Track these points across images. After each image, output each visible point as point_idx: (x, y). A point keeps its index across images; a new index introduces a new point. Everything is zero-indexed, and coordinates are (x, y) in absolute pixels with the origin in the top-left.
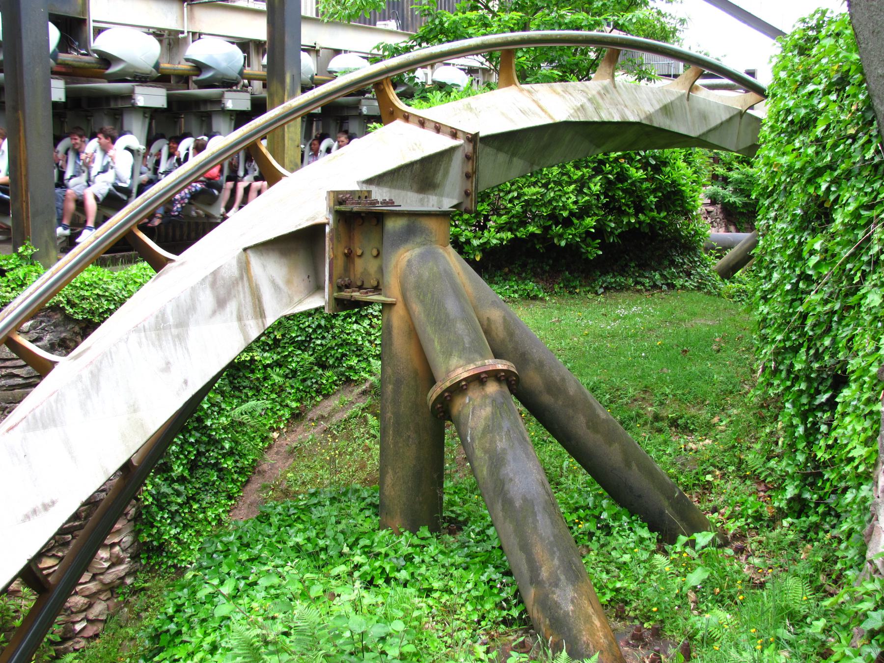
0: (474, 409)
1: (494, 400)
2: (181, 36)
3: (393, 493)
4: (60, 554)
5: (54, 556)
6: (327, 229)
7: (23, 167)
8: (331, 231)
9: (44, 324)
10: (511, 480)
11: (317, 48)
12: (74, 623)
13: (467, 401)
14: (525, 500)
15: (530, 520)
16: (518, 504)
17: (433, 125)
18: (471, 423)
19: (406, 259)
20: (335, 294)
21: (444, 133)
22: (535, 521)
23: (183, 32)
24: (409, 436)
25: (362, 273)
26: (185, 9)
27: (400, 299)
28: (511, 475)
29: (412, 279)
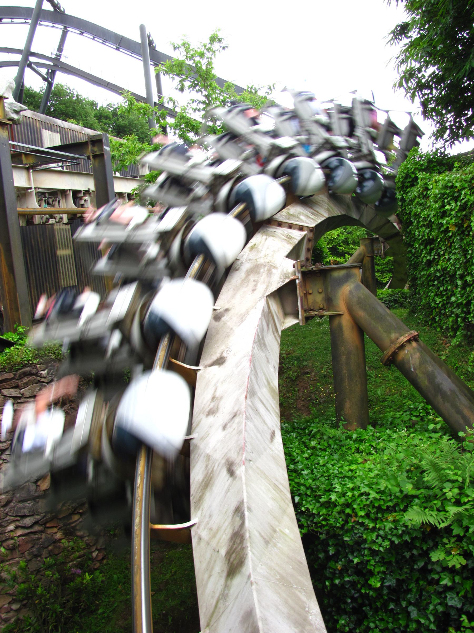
0: (411, 355)
1: (418, 350)
2: (29, 190)
3: (350, 412)
4: (81, 511)
5: (78, 513)
6: (297, 281)
7: (62, 273)
8: (299, 283)
9: (52, 371)
10: (441, 383)
11: (91, 191)
12: (92, 553)
13: (406, 352)
14: (450, 390)
15: (457, 399)
16: (449, 393)
17: (287, 225)
18: (412, 362)
19: (348, 291)
20: (305, 315)
21: (295, 229)
22: (459, 399)
23: (31, 188)
24: (357, 380)
25: (312, 303)
26: (31, 174)
27: (346, 311)
28: (441, 381)
29: (355, 299)
